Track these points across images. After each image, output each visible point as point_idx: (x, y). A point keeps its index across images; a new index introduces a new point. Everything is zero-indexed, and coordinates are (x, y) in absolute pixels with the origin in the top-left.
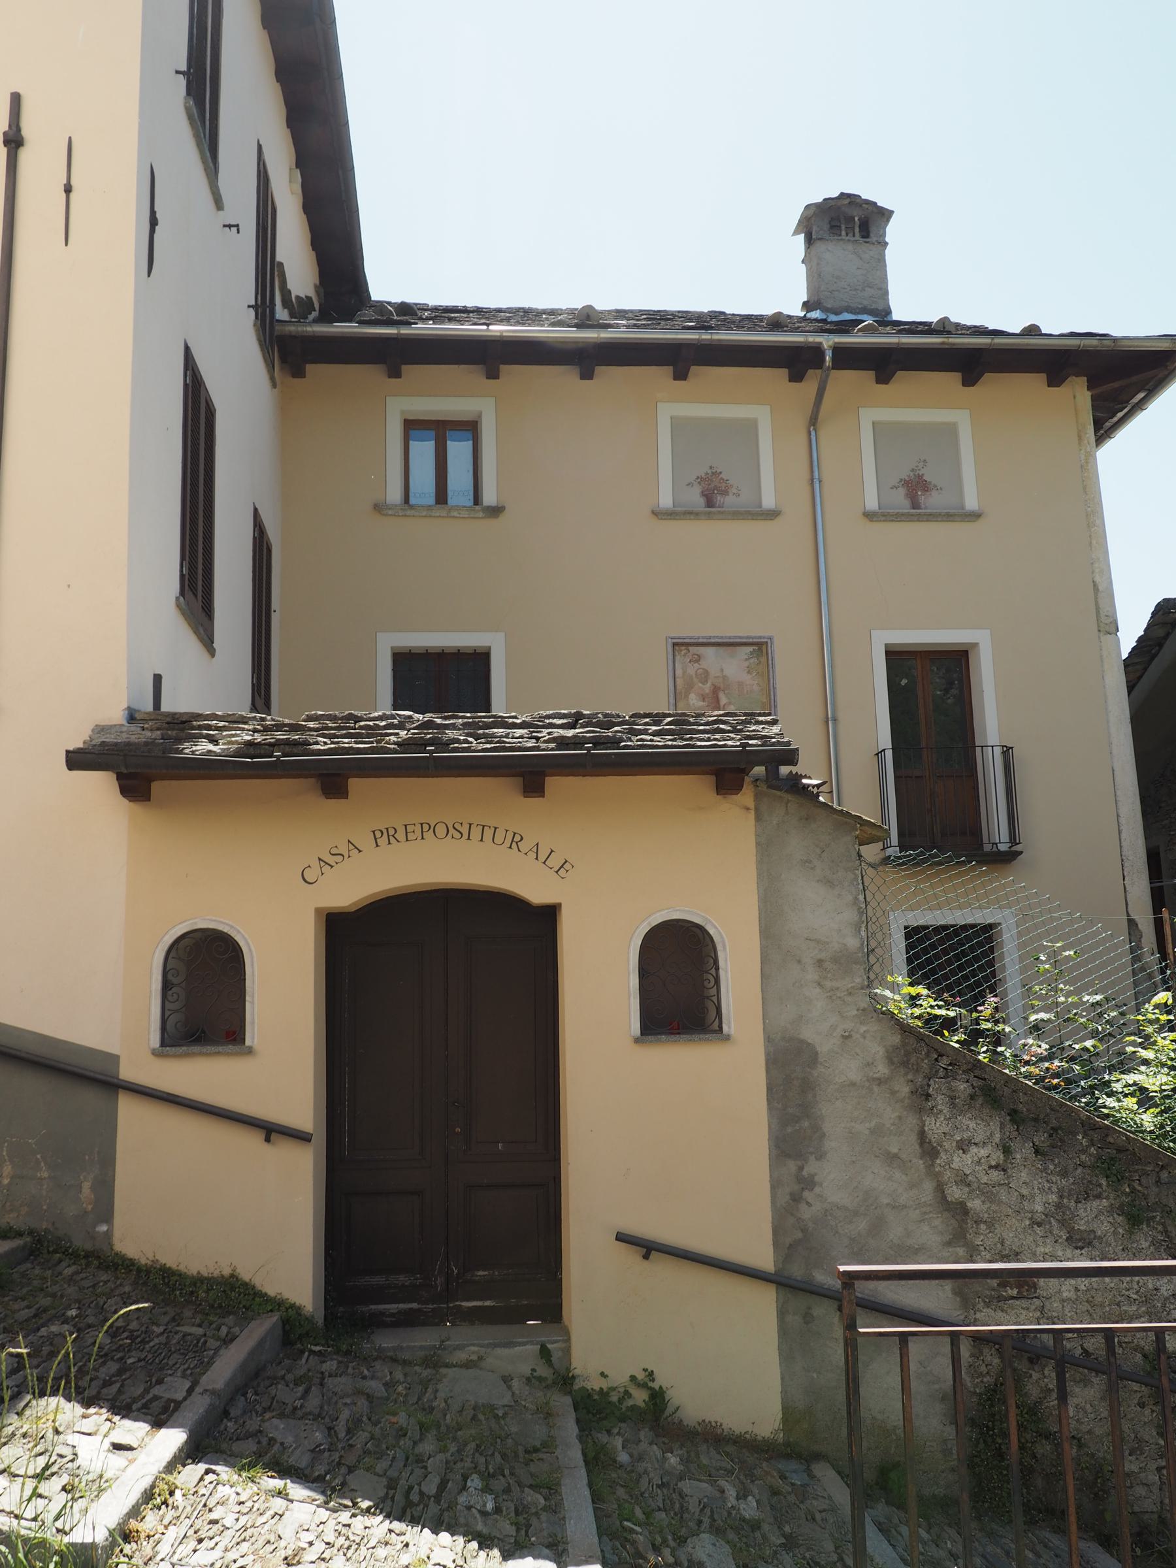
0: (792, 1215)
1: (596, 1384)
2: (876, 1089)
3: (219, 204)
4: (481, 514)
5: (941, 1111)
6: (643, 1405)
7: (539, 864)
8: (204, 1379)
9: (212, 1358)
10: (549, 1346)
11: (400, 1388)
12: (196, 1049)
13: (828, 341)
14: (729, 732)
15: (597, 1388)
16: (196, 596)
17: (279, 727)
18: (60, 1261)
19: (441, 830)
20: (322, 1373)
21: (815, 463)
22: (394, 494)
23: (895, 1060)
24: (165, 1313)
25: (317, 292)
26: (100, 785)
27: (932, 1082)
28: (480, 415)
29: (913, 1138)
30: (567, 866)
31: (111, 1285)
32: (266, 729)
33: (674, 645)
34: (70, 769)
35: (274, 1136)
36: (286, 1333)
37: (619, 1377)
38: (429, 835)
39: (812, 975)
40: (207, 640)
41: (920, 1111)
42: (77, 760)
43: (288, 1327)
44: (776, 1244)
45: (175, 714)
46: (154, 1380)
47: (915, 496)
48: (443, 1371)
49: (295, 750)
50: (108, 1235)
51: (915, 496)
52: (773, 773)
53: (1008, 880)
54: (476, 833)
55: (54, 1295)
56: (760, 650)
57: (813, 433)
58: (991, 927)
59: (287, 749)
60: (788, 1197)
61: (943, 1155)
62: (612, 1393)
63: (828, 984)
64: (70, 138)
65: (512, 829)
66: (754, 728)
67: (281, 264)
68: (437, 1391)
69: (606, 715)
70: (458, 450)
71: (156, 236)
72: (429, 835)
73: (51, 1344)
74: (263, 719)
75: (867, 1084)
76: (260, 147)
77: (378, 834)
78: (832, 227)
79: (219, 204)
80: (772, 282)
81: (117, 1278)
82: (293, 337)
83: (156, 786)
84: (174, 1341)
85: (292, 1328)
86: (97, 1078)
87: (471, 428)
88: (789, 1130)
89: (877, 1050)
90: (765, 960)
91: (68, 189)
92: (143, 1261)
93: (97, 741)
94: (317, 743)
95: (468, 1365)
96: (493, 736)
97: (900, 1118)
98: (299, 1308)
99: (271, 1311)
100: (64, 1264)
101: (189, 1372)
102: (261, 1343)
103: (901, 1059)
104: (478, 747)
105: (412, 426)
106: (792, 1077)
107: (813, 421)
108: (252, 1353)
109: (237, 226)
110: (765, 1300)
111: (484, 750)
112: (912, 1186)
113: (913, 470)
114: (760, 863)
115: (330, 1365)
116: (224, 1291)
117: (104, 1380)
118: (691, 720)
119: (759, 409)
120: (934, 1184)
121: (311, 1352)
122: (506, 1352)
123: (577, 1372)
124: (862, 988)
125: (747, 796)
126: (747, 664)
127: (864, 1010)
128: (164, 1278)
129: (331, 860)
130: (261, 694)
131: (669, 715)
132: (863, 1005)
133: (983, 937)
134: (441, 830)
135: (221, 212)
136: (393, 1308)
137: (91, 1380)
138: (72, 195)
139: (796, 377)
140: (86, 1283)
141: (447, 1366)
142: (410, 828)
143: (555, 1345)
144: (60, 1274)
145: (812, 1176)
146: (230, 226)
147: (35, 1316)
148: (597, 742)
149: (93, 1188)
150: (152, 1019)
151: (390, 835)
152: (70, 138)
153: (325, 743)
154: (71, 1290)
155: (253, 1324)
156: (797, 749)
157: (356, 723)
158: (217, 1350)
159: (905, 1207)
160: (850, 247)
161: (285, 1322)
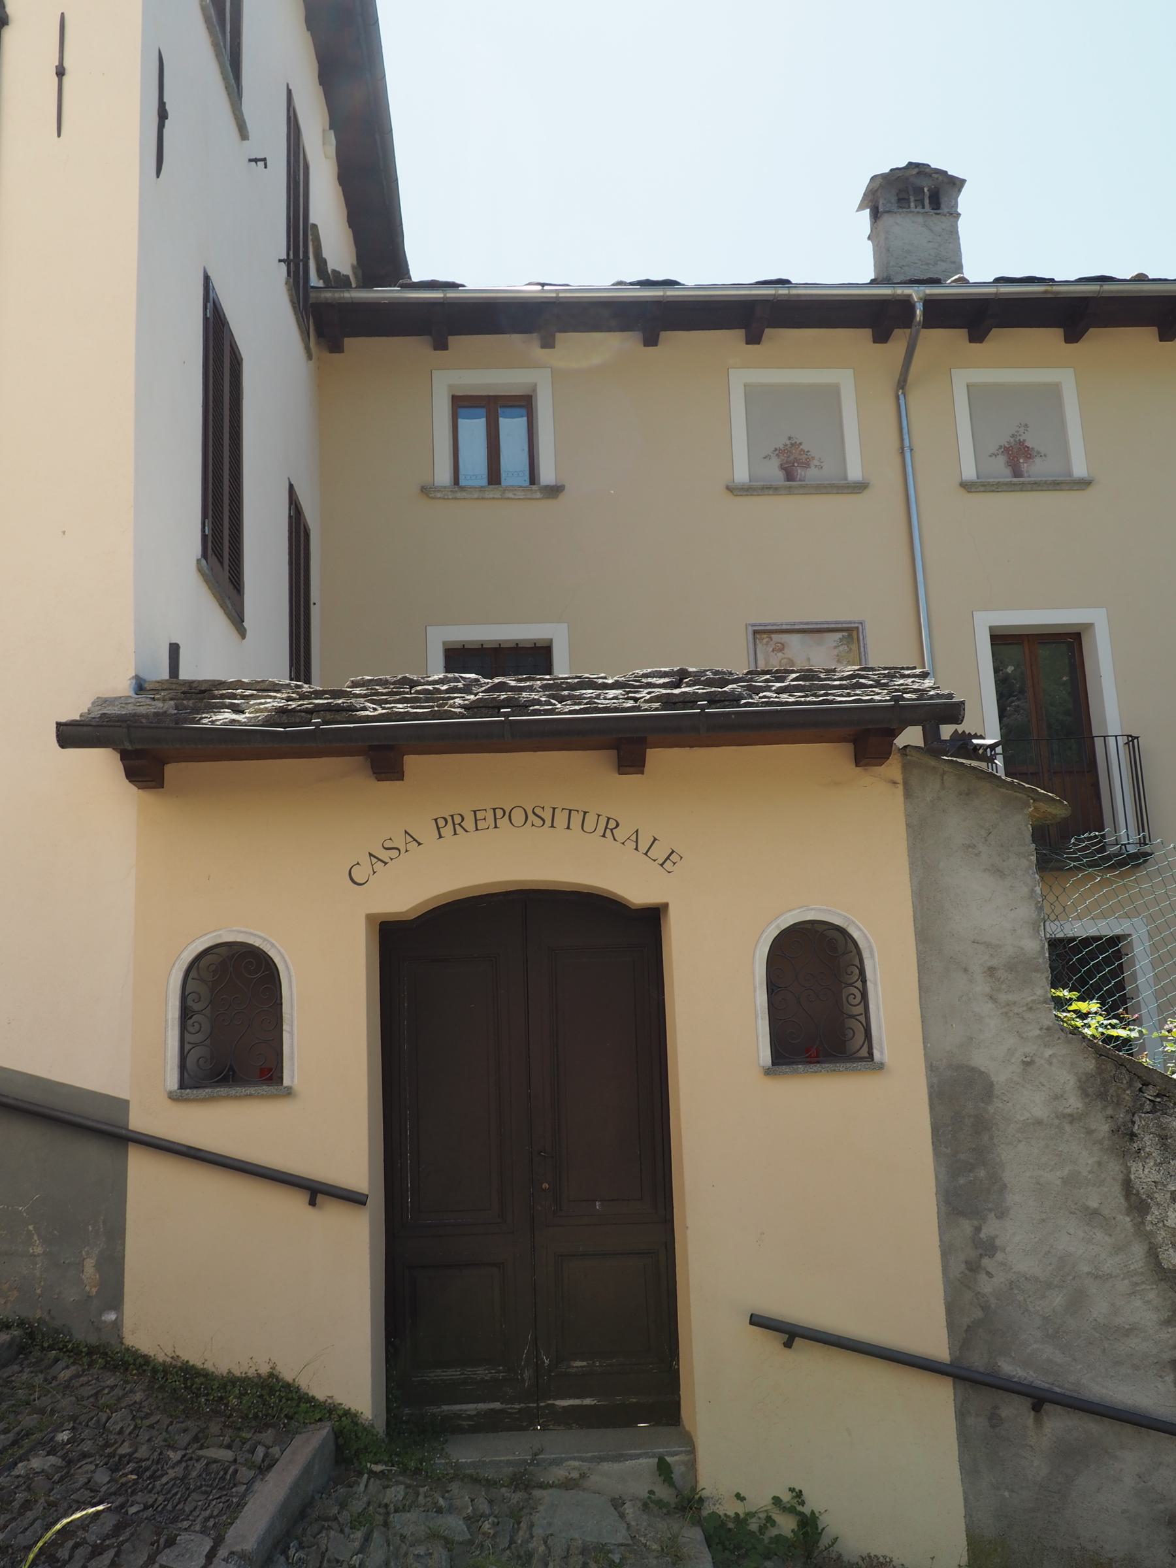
0: (969, 1288)
1: (730, 1508)
2: (1067, 1128)
3: (243, 133)
4: (538, 495)
5: (1150, 1154)
6: (790, 1535)
7: (640, 855)
8: (231, 1533)
9: (244, 1496)
10: (669, 1459)
11: (486, 1526)
12: (223, 1091)
13: (916, 293)
14: (871, 686)
15: (731, 1514)
16: (222, 563)
17: (318, 694)
18: (57, 1360)
19: (518, 817)
20: (386, 1506)
21: (905, 431)
22: (443, 476)
23: (1090, 1090)
24: (185, 1431)
25: (355, 273)
26: (100, 765)
27: (1136, 1118)
28: (535, 390)
29: (1117, 1190)
30: (674, 857)
31: (118, 1392)
32: (303, 696)
33: (755, 632)
34: (62, 747)
35: (320, 1198)
36: (339, 1449)
37: (759, 1500)
38: (503, 823)
39: (981, 986)
40: (237, 618)
41: (1124, 1154)
42: (70, 735)
43: (341, 1441)
44: (951, 1325)
45: (193, 682)
46: (162, 1541)
47: (1018, 465)
48: (537, 1493)
49: (338, 718)
50: (117, 1325)
51: (1018, 465)
52: (931, 735)
53: (1140, 884)
54: (561, 818)
55: (42, 1412)
56: (850, 636)
57: (902, 397)
58: (1115, 940)
59: (329, 716)
60: (963, 1266)
61: (1156, 1211)
62: (754, 1520)
63: (1003, 997)
64: (63, 14)
65: (606, 813)
66: (901, 681)
67: (315, 226)
68: (532, 1525)
69: (716, 673)
70: (512, 428)
71: (165, 131)
72: (503, 823)
73: (29, 1489)
74: (298, 687)
75: (1056, 1122)
76: (289, 92)
77: (441, 823)
78: (899, 200)
79: (243, 133)
80: (843, 258)
81: (127, 1382)
82: (330, 306)
83: (170, 770)
84: (194, 1474)
85: (347, 1443)
86: (95, 1129)
87: (525, 403)
88: (962, 1181)
89: (1066, 1079)
90: (923, 967)
91: (61, 72)
92: (161, 1358)
93: (96, 713)
94: (365, 709)
95: (568, 1485)
96: (580, 697)
97: (1099, 1164)
98: (355, 1415)
99: (320, 1420)
100: (61, 1364)
101: (211, 1523)
102: (307, 1470)
103: (1096, 1090)
104: (565, 710)
105: (461, 404)
106: (962, 1113)
107: (902, 384)
108: (295, 1487)
109: (264, 160)
110: (940, 1397)
111: (571, 712)
112: (1118, 1249)
113: (1013, 436)
114: (912, 849)
115: (395, 1493)
116: (261, 1396)
117: (95, 1546)
118: (822, 675)
119: (843, 371)
120: (1146, 1247)
121: (372, 1473)
122: (616, 1466)
123: (705, 1493)
124: (1045, 1002)
125: (893, 768)
126: (836, 652)
127: (1048, 1029)
128: (186, 1380)
129: (384, 855)
130: (300, 665)
131: (793, 672)
132: (1048, 1023)
133: (1114, 946)
134: (518, 817)
135: (246, 142)
136: (470, 1408)
137: (76, 1546)
138: (66, 79)
139: (881, 337)
140: (87, 1391)
141: (542, 1486)
142: (480, 815)
143: (677, 1458)
144: (55, 1378)
145: (992, 1239)
146: (256, 160)
147: (15, 1443)
148: (713, 700)
149: (98, 1267)
150: (169, 1054)
151: (456, 823)
152: (63, 14)
153: (375, 709)
154: (66, 1403)
155: (298, 1440)
156: (963, 703)
157: (411, 688)
158: (250, 1484)
159: (1110, 1276)
160: (920, 219)
161: (338, 1434)
